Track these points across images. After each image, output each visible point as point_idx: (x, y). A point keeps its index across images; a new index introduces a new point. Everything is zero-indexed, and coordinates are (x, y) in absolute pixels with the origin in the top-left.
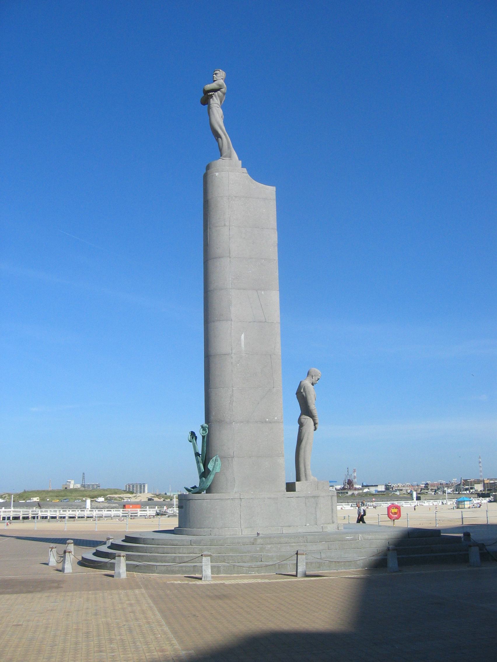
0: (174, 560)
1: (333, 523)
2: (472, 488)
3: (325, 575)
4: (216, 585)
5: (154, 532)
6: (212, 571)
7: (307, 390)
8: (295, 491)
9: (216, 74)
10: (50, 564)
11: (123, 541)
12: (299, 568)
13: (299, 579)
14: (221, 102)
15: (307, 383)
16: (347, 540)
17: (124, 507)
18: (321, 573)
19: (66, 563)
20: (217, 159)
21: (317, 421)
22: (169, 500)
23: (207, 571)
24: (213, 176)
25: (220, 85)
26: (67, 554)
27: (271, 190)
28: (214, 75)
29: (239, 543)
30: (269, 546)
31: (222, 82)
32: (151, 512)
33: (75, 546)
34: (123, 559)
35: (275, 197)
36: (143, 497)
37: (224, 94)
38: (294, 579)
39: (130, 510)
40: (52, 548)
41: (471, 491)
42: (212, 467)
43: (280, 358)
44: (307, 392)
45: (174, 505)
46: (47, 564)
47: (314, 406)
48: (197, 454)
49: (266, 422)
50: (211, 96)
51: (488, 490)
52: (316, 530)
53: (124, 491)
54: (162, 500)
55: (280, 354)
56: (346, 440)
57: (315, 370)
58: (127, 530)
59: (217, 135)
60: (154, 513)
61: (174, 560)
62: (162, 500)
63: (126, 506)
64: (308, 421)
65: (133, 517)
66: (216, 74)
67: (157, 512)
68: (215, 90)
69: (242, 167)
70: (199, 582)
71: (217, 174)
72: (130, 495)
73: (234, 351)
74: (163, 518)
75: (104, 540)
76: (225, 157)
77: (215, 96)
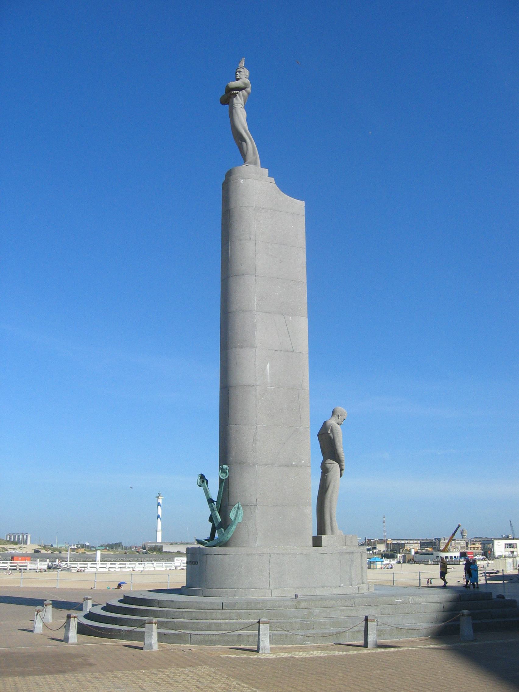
0: (209, 627)
1: (363, 583)
2: (375, 548)
3: (396, 645)
4: (278, 659)
5: (149, 591)
6: (270, 641)
7: (335, 431)
8: (321, 546)
9: (239, 72)
10: (36, 631)
11: (120, 601)
12: (369, 636)
13: (371, 650)
14: (244, 103)
15: (333, 422)
16: (397, 603)
17: (12, 559)
18: (392, 642)
19: (71, 630)
20: (241, 165)
21: (344, 467)
22: (57, 552)
23: (265, 642)
24: (236, 183)
25: (245, 84)
26: (72, 619)
27: (299, 205)
28: (238, 73)
29: (280, 607)
30: (317, 611)
31: (247, 81)
32: (42, 565)
33: (55, 609)
34: (154, 626)
35: (304, 213)
36: (29, 548)
37: (249, 94)
38: (363, 651)
39: (18, 563)
40: (38, 611)
41: (374, 551)
42: (234, 516)
43: (308, 392)
44: (335, 434)
45: (67, 558)
46: (32, 631)
47: (342, 449)
48: (210, 501)
49: (292, 465)
50: (235, 95)
51: (391, 551)
52: (351, 592)
53: (8, 541)
54: (50, 552)
55: (308, 388)
56: (380, 489)
57: (341, 409)
58: (22, 586)
59: (239, 138)
60: (45, 567)
61: (209, 627)
62: (50, 552)
63: (15, 558)
64: (333, 466)
65: (23, 570)
66: (239, 72)
67: (48, 566)
68: (240, 89)
69: (269, 176)
70: (255, 656)
71: (242, 181)
72: (15, 547)
73: (258, 383)
74: (55, 572)
75: (80, 600)
76: (250, 163)
77: (239, 96)
